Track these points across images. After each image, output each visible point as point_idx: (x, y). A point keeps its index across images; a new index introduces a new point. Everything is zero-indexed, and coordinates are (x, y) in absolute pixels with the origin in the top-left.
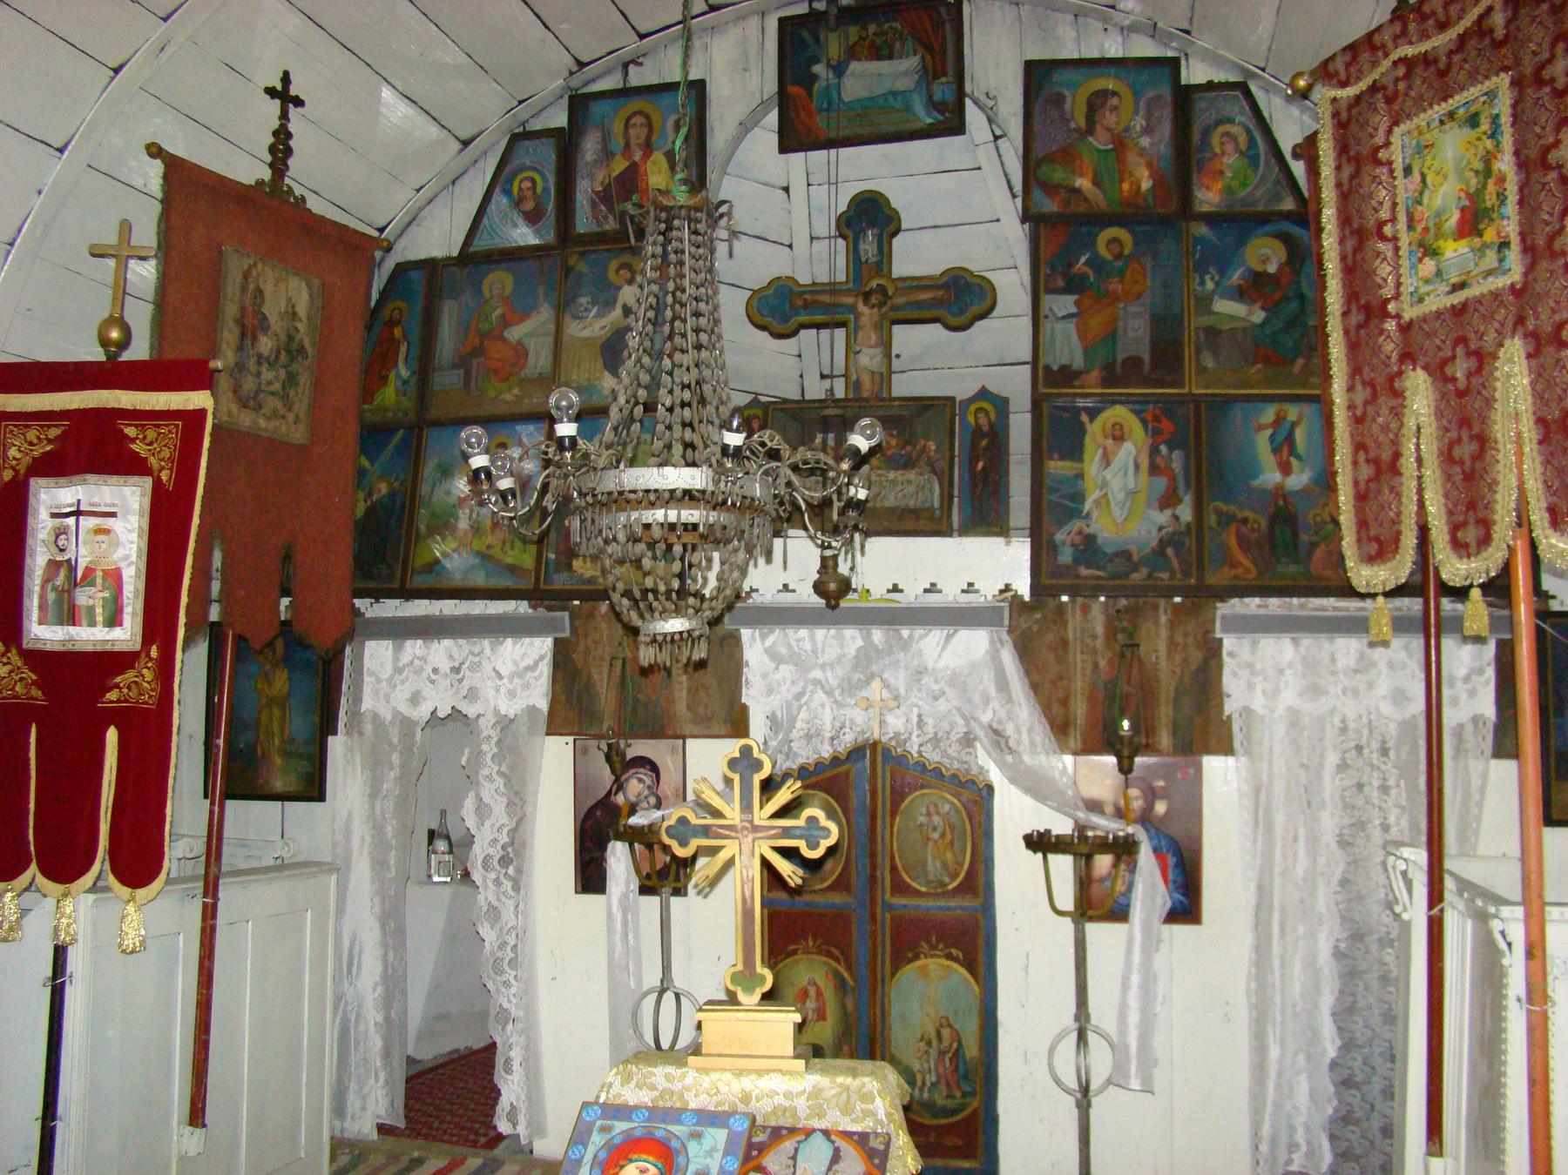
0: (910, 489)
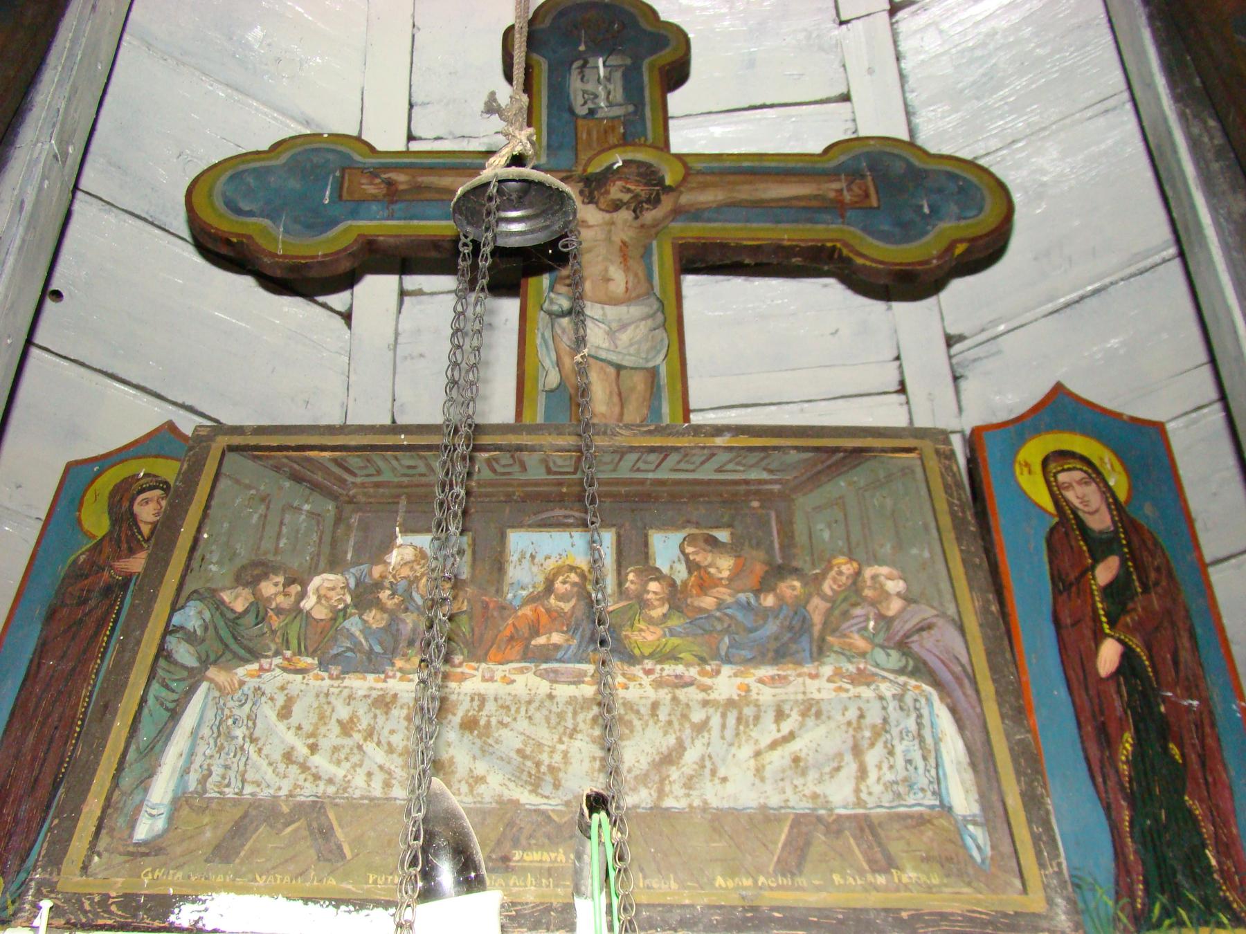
0: (815, 739)
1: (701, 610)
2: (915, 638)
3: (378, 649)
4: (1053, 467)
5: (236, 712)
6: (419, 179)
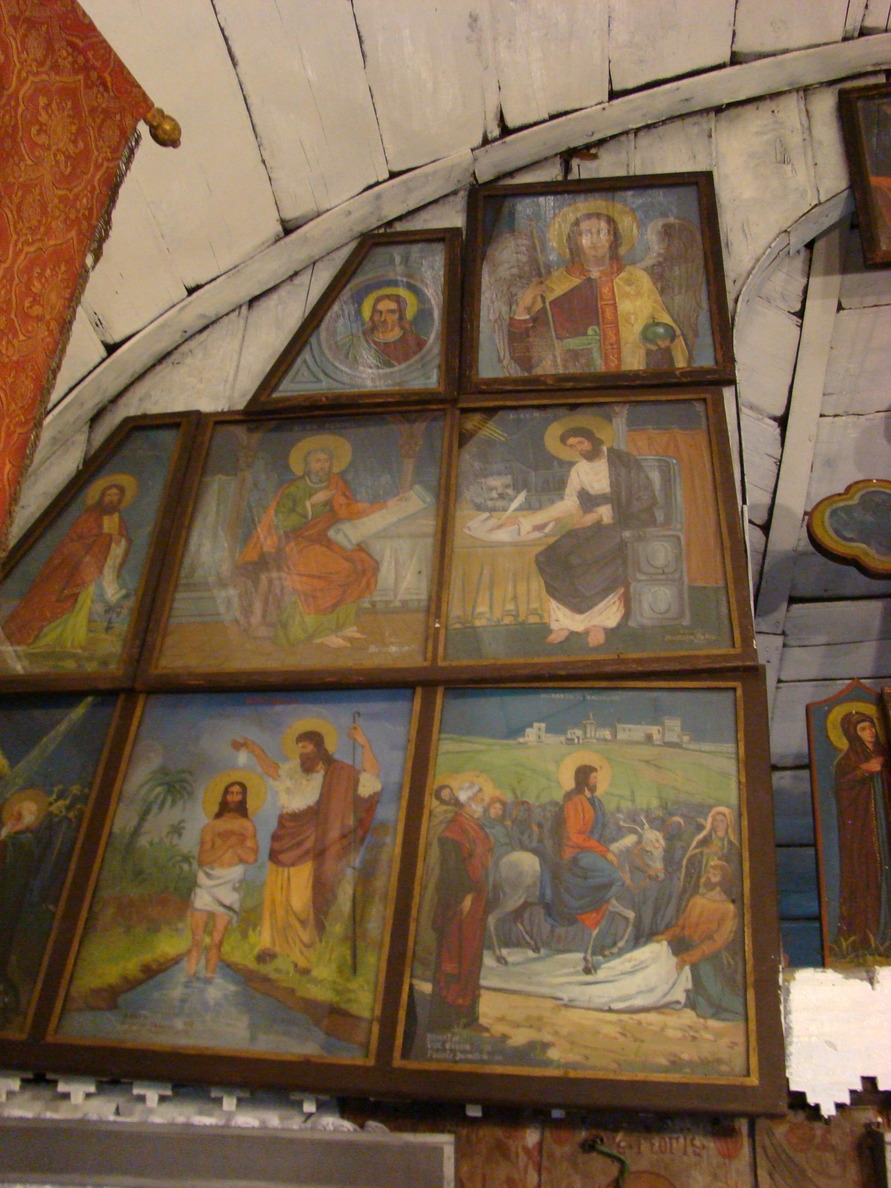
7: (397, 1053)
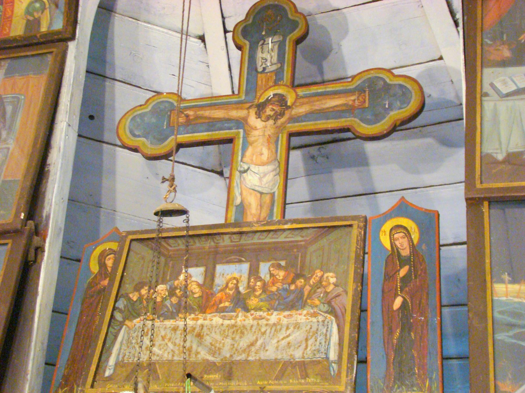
1: (272, 292)
2: (334, 300)
3: (174, 311)
4: (393, 232)
5: (133, 335)
6: (198, 113)
7: (478, 183)
